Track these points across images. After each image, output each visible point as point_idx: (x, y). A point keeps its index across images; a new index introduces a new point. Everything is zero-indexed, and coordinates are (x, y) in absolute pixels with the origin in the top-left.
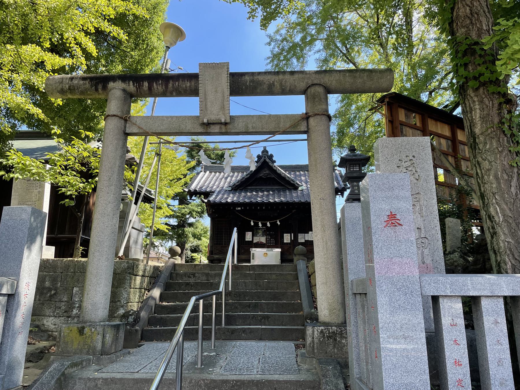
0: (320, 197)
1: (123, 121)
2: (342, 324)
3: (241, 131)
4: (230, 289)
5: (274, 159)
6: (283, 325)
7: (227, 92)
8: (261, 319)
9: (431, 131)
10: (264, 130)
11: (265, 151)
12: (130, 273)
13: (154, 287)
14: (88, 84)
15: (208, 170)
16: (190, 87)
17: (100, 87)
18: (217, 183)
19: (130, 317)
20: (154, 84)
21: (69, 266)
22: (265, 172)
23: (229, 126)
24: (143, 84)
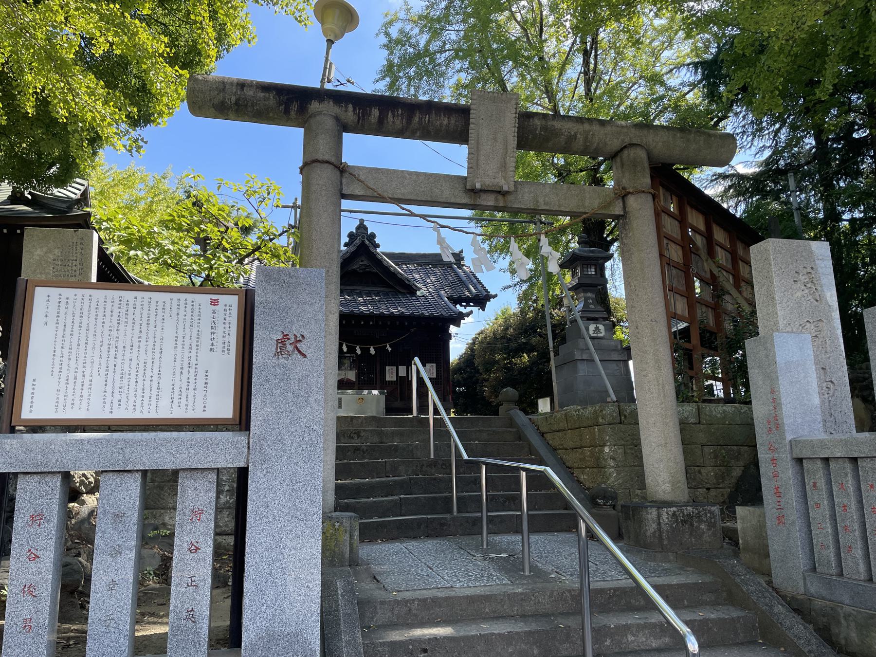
0: (650, 318)
1: (338, 173)
4: (432, 457)
5: (377, 240)
6: (536, 510)
8: (505, 502)
10: (562, 209)
11: (362, 227)
16: (448, 126)
17: (295, 107)
22: (361, 263)
23: (510, 198)
24: (370, 111)
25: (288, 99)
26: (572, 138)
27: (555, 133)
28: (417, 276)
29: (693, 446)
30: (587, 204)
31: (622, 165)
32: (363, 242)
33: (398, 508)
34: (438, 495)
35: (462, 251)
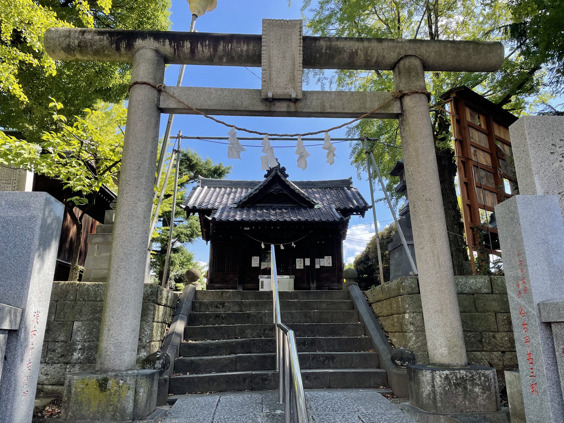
1: (156, 92)
2: (466, 366)
3: (316, 110)
5: (286, 172)
6: (352, 368)
7: (299, 59)
9: (496, 136)
10: (346, 111)
12: (153, 301)
13: (177, 320)
14: (105, 40)
15: (206, 185)
16: (247, 50)
17: (123, 45)
18: (218, 200)
19: (158, 362)
20: (199, 45)
21: (68, 292)
23: (300, 104)
24: (183, 43)
25: (117, 39)
26: (353, 54)
27: (339, 51)
28: (317, 196)
29: (487, 314)
30: (368, 105)
31: (400, 73)
32: (276, 173)
33: (233, 365)
34: (267, 354)
35: (351, 178)
